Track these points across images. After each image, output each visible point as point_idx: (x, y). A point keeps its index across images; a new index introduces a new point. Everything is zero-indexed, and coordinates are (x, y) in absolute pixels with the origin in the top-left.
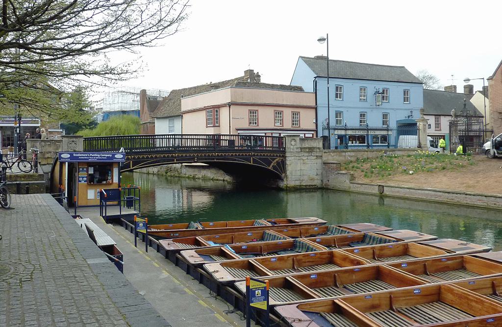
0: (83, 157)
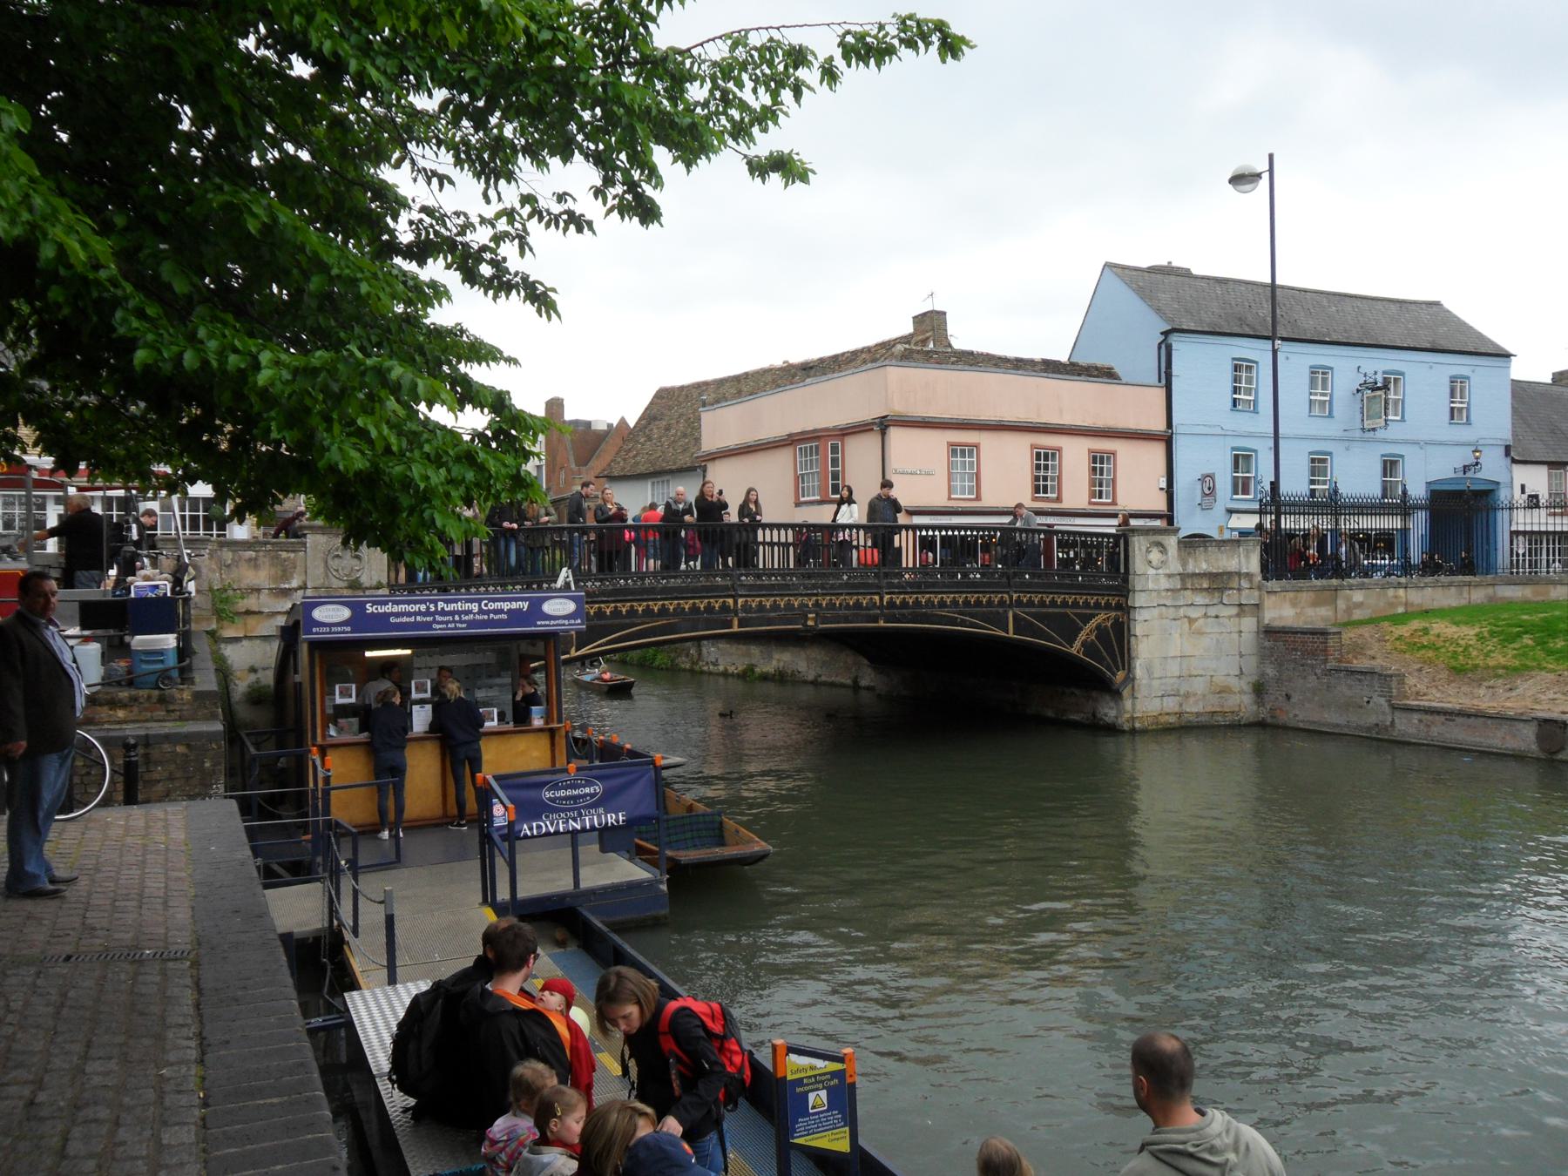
0: (409, 614)
